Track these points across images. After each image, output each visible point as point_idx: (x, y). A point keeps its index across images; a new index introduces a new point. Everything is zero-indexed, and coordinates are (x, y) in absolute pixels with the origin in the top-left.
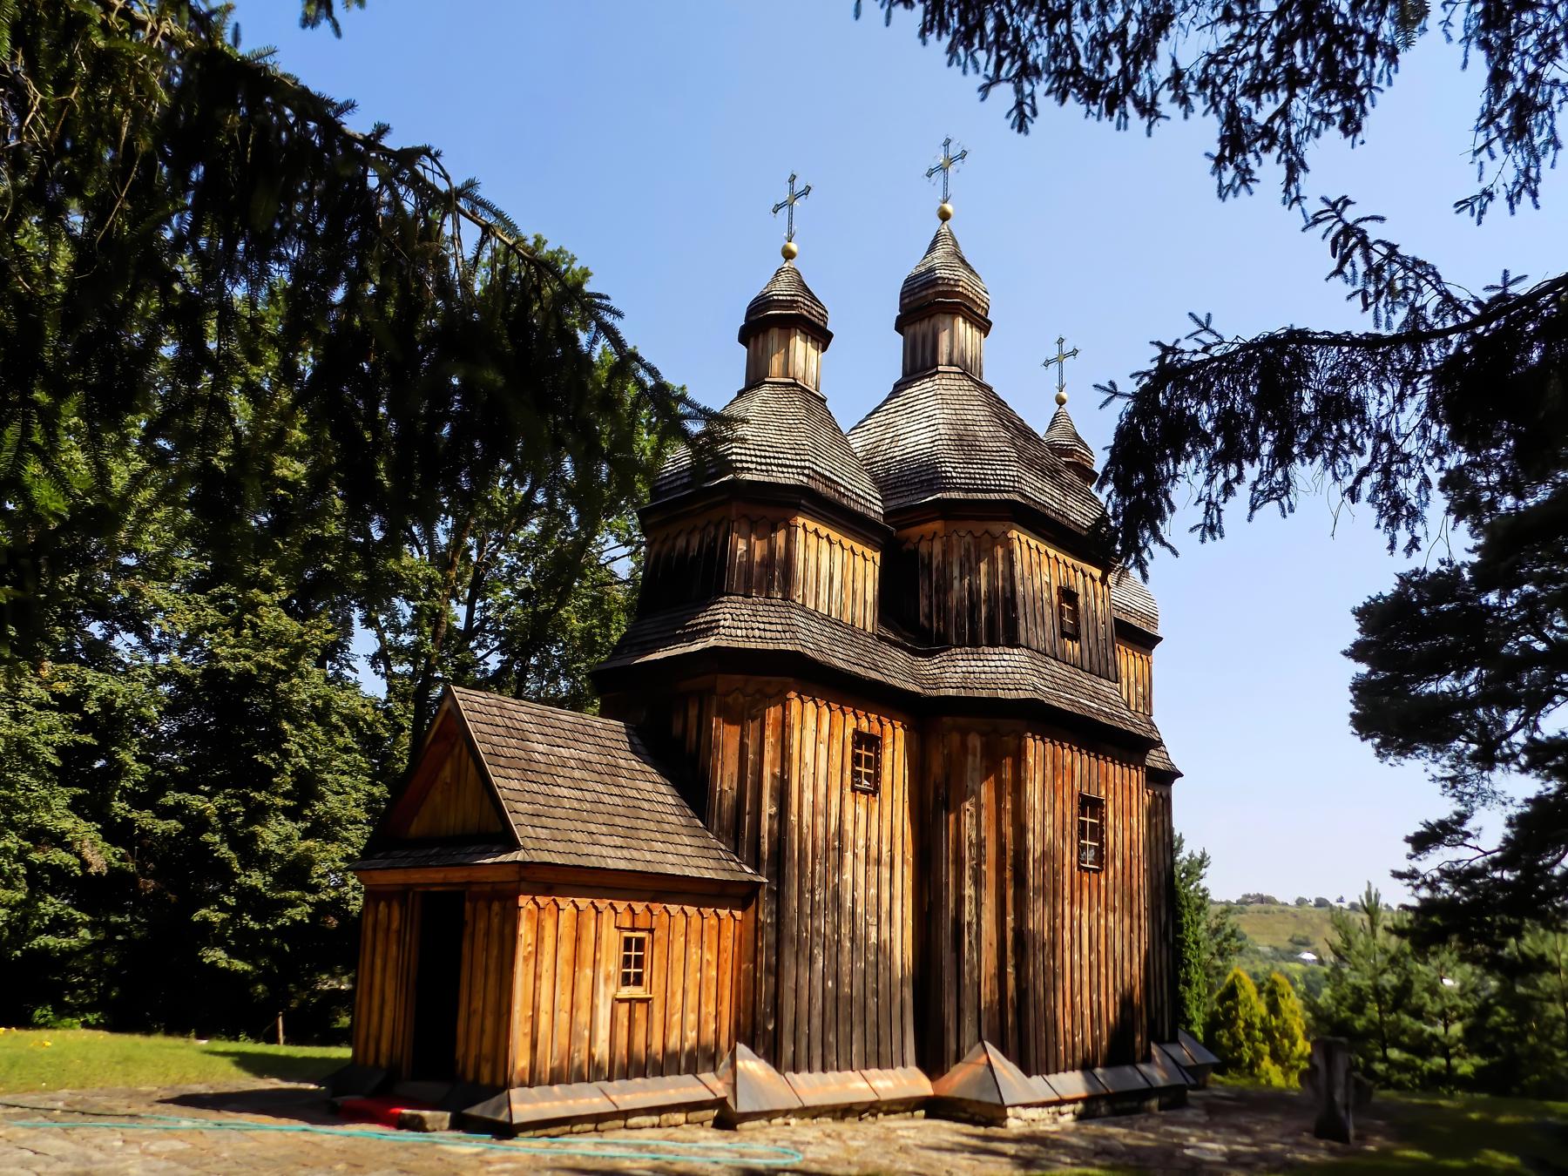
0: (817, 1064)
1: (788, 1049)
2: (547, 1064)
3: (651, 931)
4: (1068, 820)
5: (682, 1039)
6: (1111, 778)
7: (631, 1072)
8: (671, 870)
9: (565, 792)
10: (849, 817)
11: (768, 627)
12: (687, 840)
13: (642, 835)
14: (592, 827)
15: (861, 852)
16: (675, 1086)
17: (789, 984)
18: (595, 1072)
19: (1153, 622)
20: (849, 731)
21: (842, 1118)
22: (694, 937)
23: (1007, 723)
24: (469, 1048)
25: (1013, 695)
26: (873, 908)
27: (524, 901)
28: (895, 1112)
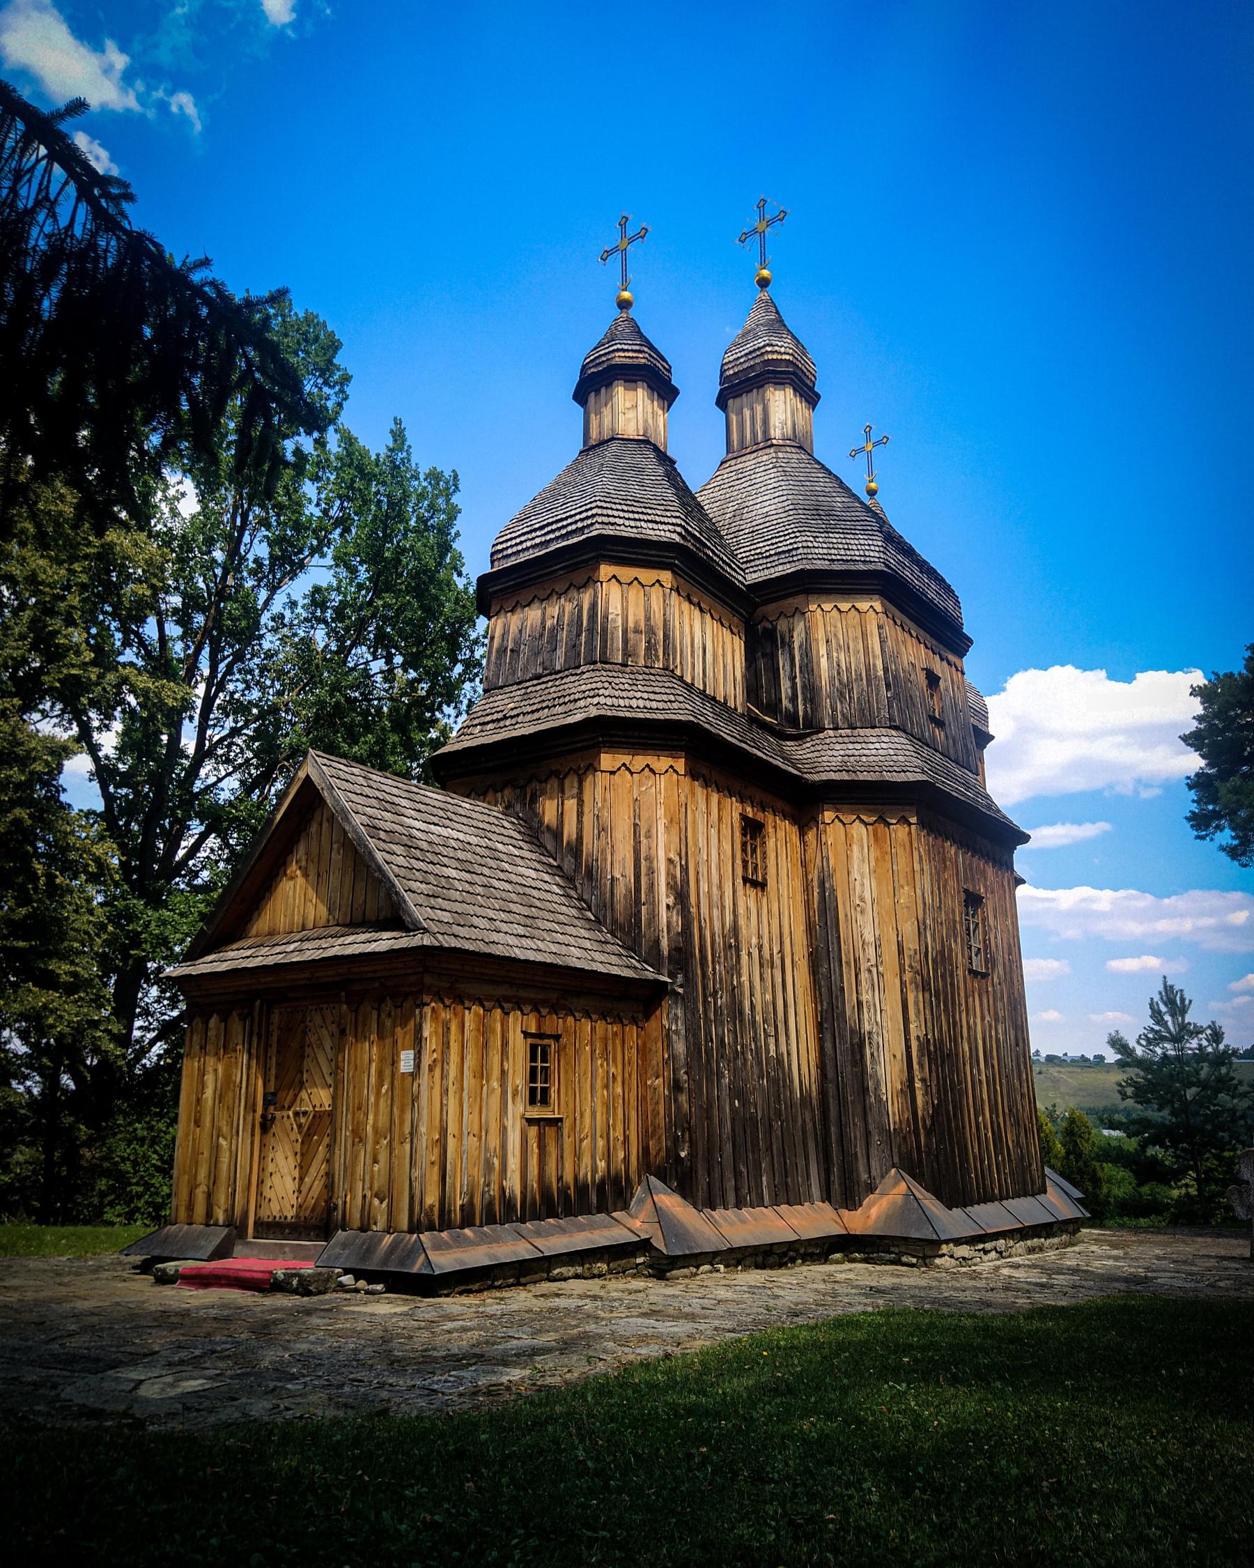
0: (731, 1198)
5: (594, 1170)
9: (454, 873)
10: (741, 910)
11: (652, 696)
12: (583, 933)
18: (501, 1212)
25: (901, 778)
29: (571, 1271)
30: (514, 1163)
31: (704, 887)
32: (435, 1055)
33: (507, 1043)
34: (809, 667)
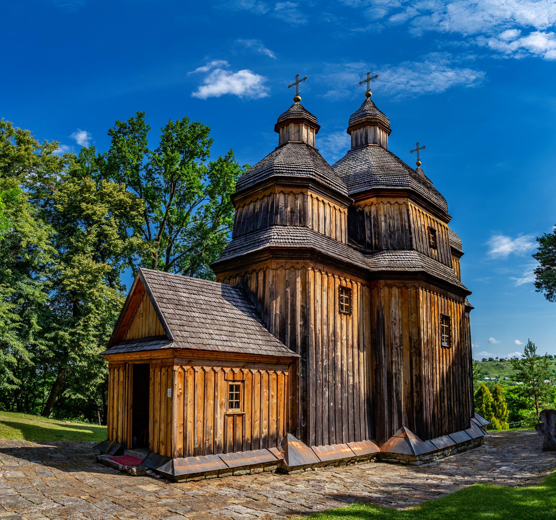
0: (326, 441)
1: (312, 437)
2: (191, 447)
3: (243, 381)
4: (437, 326)
5: (261, 432)
6: (452, 307)
7: (235, 449)
8: (251, 351)
9: (197, 315)
10: (338, 326)
11: (295, 238)
12: (260, 337)
13: (237, 335)
14: (211, 331)
15: (345, 342)
16: (258, 455)
17: (312, 405)
19: (460, 246)
20: (337, 286)
21: (339, 466)
22: (265, 384)
23: (411, 280)
24: (155, 436)
26: (350, 368)
27: (176, 368)
28: (363, 461)
29: (244, 472)
30: (220, 432)
31: (319, 316)
32: (181, 391)
33: (217, 385)
34: (377, 225)
